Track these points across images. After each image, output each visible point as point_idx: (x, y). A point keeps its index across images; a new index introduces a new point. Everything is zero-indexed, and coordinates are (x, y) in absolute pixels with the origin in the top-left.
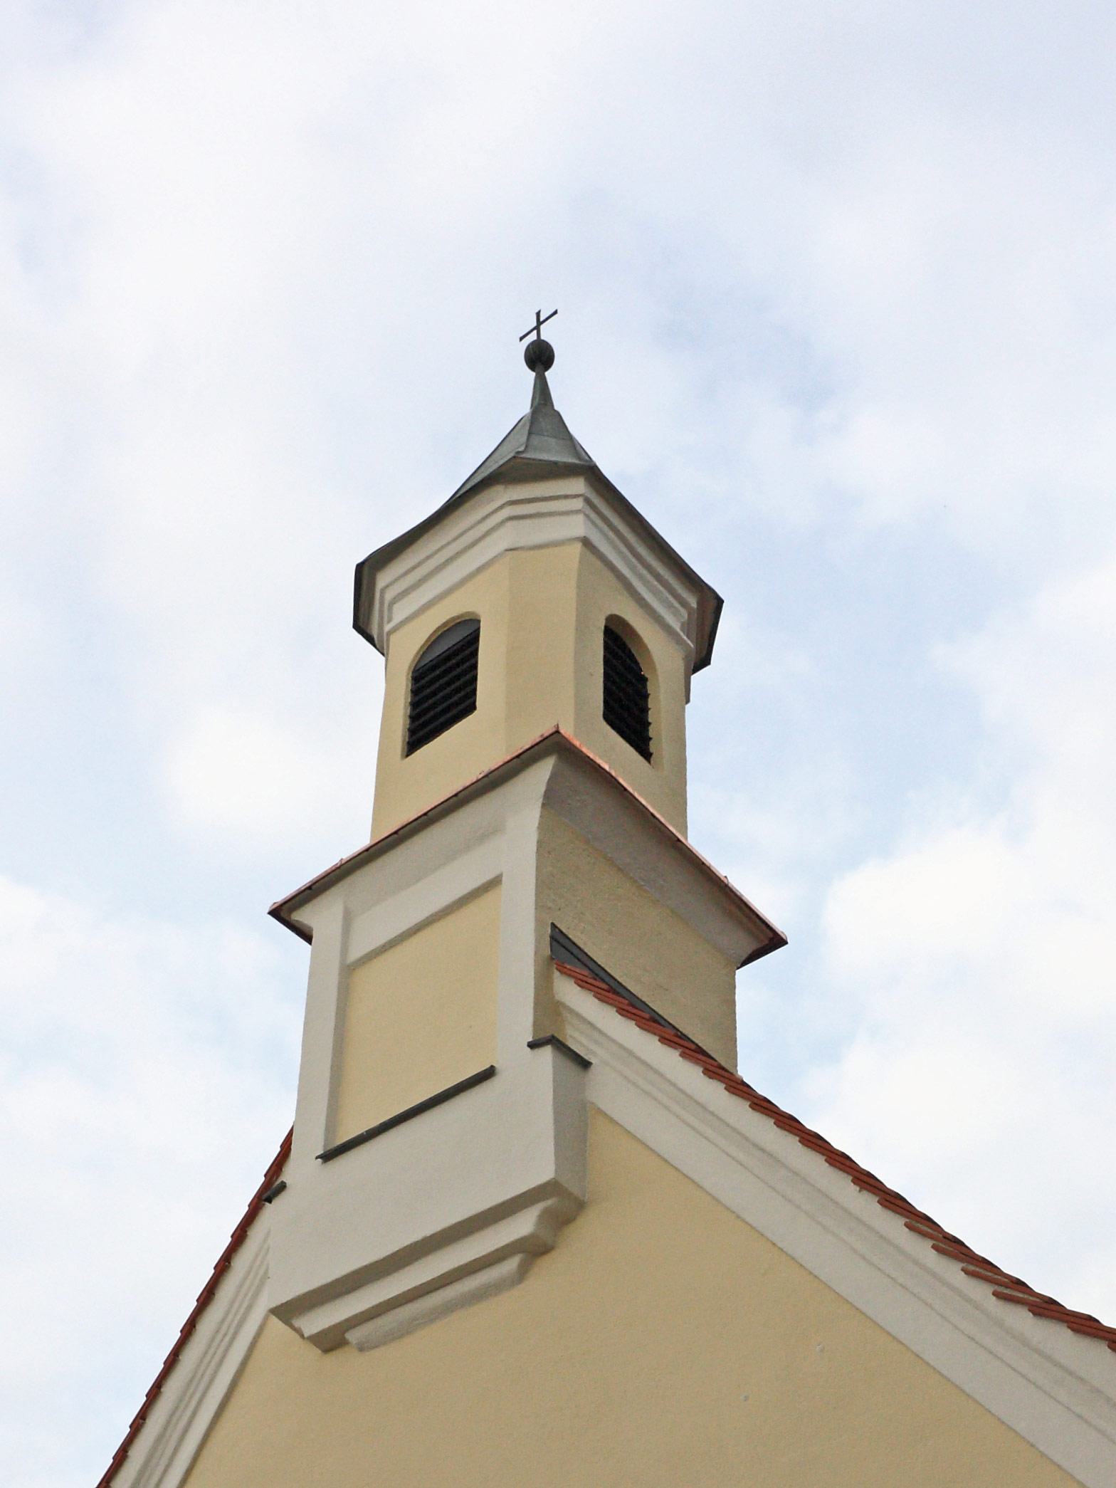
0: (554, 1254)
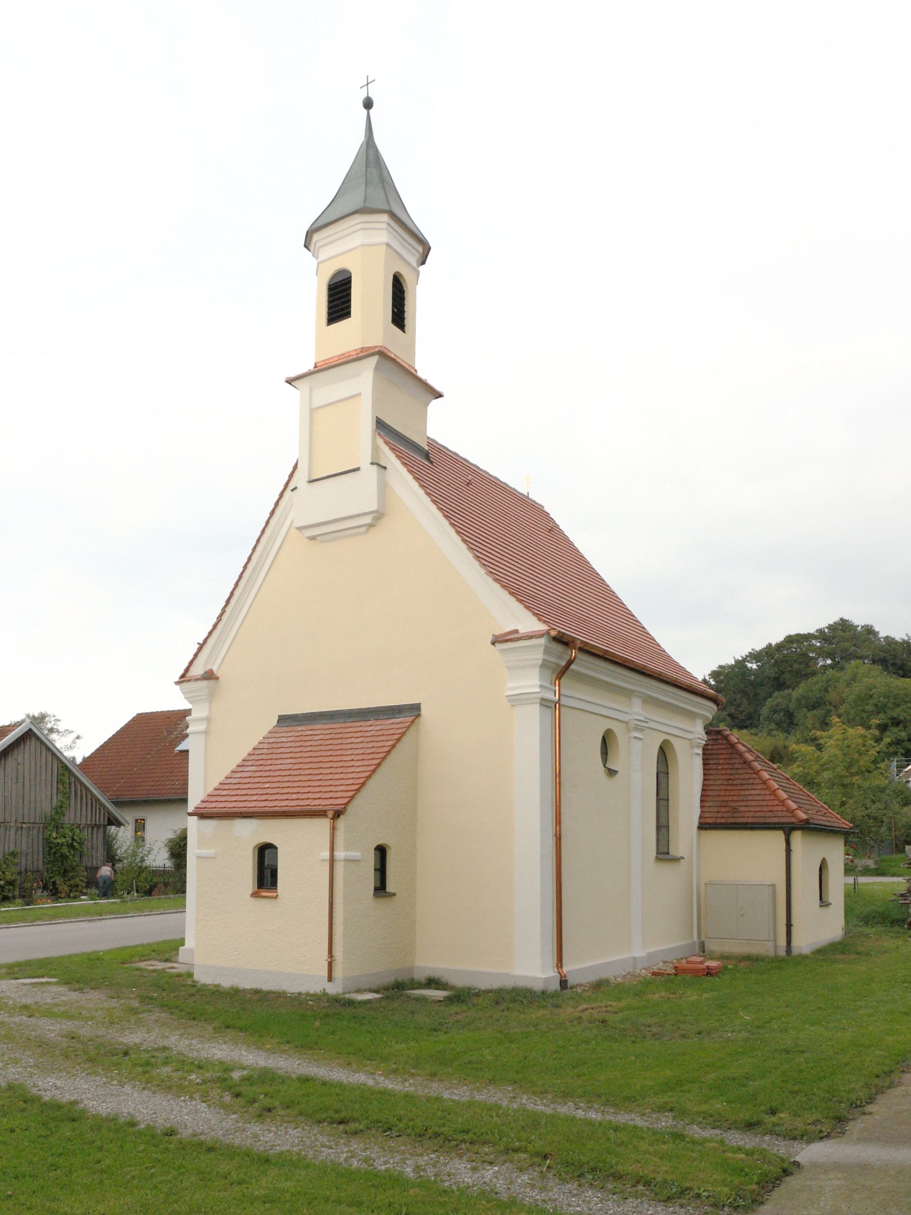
0: (375, 527)
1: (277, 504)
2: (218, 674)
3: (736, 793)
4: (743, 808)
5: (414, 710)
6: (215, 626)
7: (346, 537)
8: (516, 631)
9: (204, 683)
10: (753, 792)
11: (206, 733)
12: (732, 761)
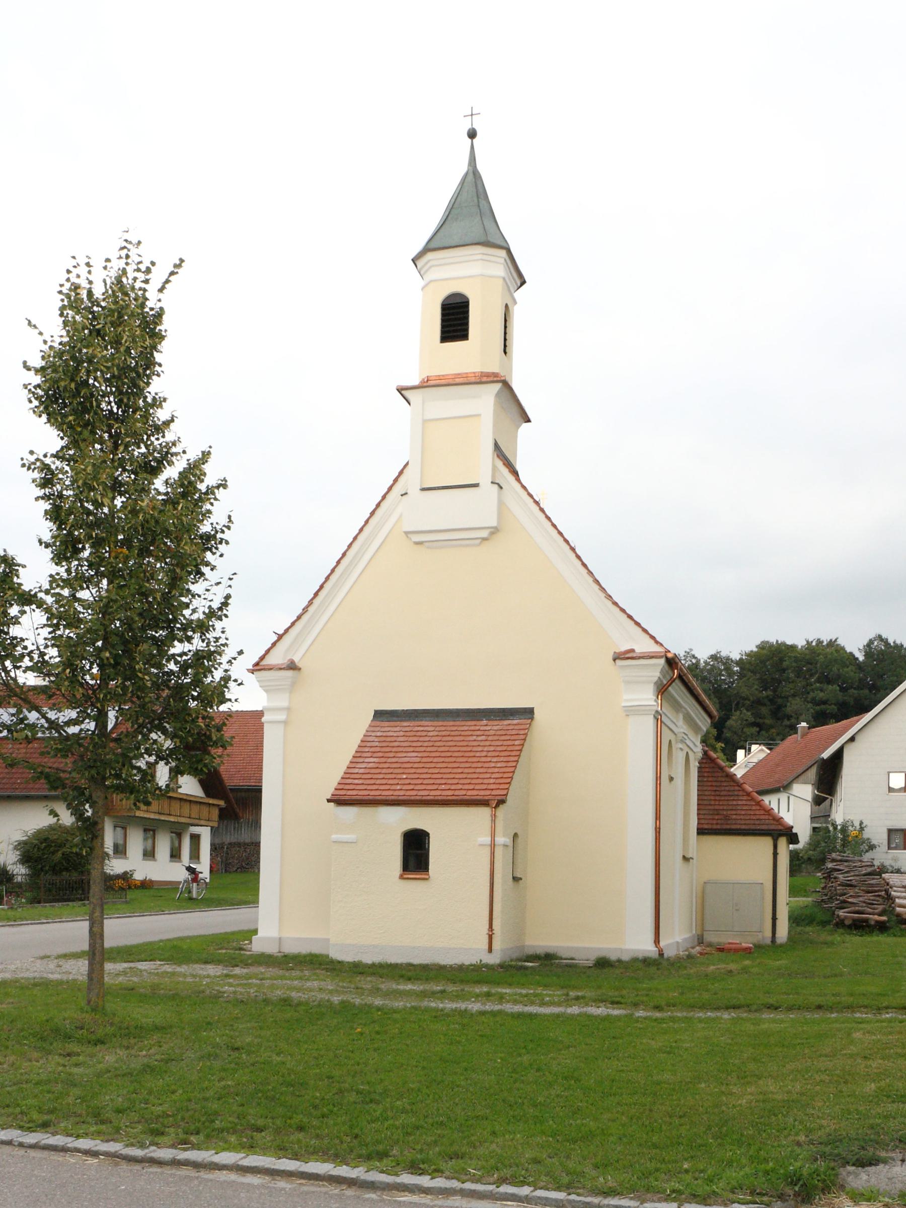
1: (378, 505)
2: (299, 665)
3: (725, 803)
4: (734, 817)
5: (529, 713)
6: (299, 618)
7: (467, 546)
8: (633, 651)
9: (290, 673)
10: (740, 803)
11: (285, 723)
12: (715, 775)
